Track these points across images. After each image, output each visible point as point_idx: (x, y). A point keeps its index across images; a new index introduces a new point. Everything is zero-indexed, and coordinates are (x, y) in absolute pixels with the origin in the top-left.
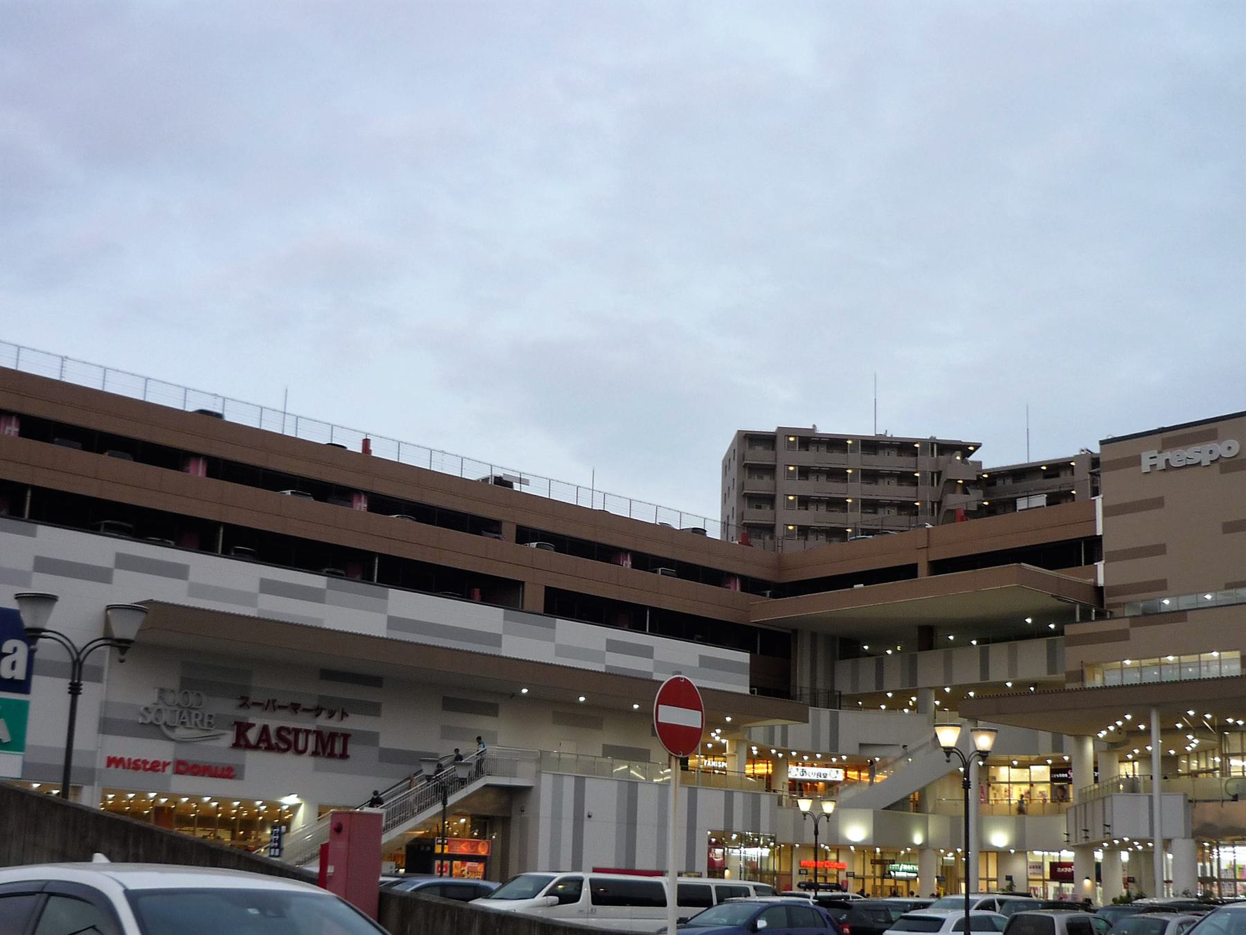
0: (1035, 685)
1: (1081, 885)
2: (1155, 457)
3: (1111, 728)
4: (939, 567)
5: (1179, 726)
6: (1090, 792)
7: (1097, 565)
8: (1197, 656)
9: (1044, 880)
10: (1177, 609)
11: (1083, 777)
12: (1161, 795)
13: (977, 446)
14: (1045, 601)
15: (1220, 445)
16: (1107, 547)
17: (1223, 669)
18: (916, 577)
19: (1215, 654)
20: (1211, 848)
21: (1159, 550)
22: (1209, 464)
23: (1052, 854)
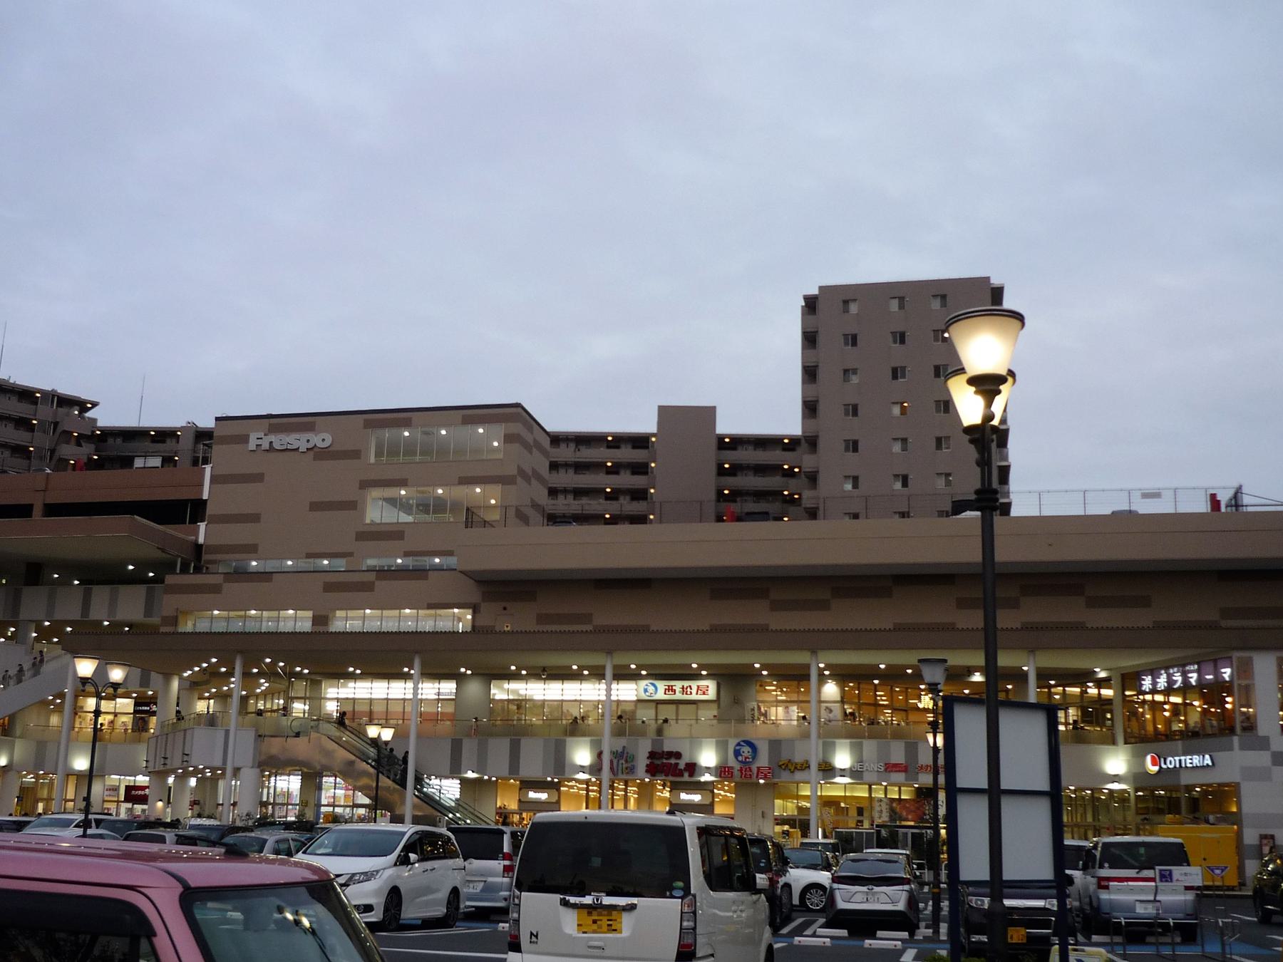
0: (130, 626)
1: (153, 807)
2: (261, 438)
3: (197, 669)
4: (53, 510)
5: (255, 670)
6: (168, 725)
7: (199, 525)
8: (277, 612)
9: (118, 802)
10: (263, 571)
11: (167, 709)
12: (236, 730)
13: (95, 405)
14: (149, 551)
15: (316, 436)
16: (210, 510)
17: (297, 625)
18: (31, 516)
19: (291, 612)
20: (270, 776)
21: (255, 518)
22: (305, 450)
23: (128, 778)
